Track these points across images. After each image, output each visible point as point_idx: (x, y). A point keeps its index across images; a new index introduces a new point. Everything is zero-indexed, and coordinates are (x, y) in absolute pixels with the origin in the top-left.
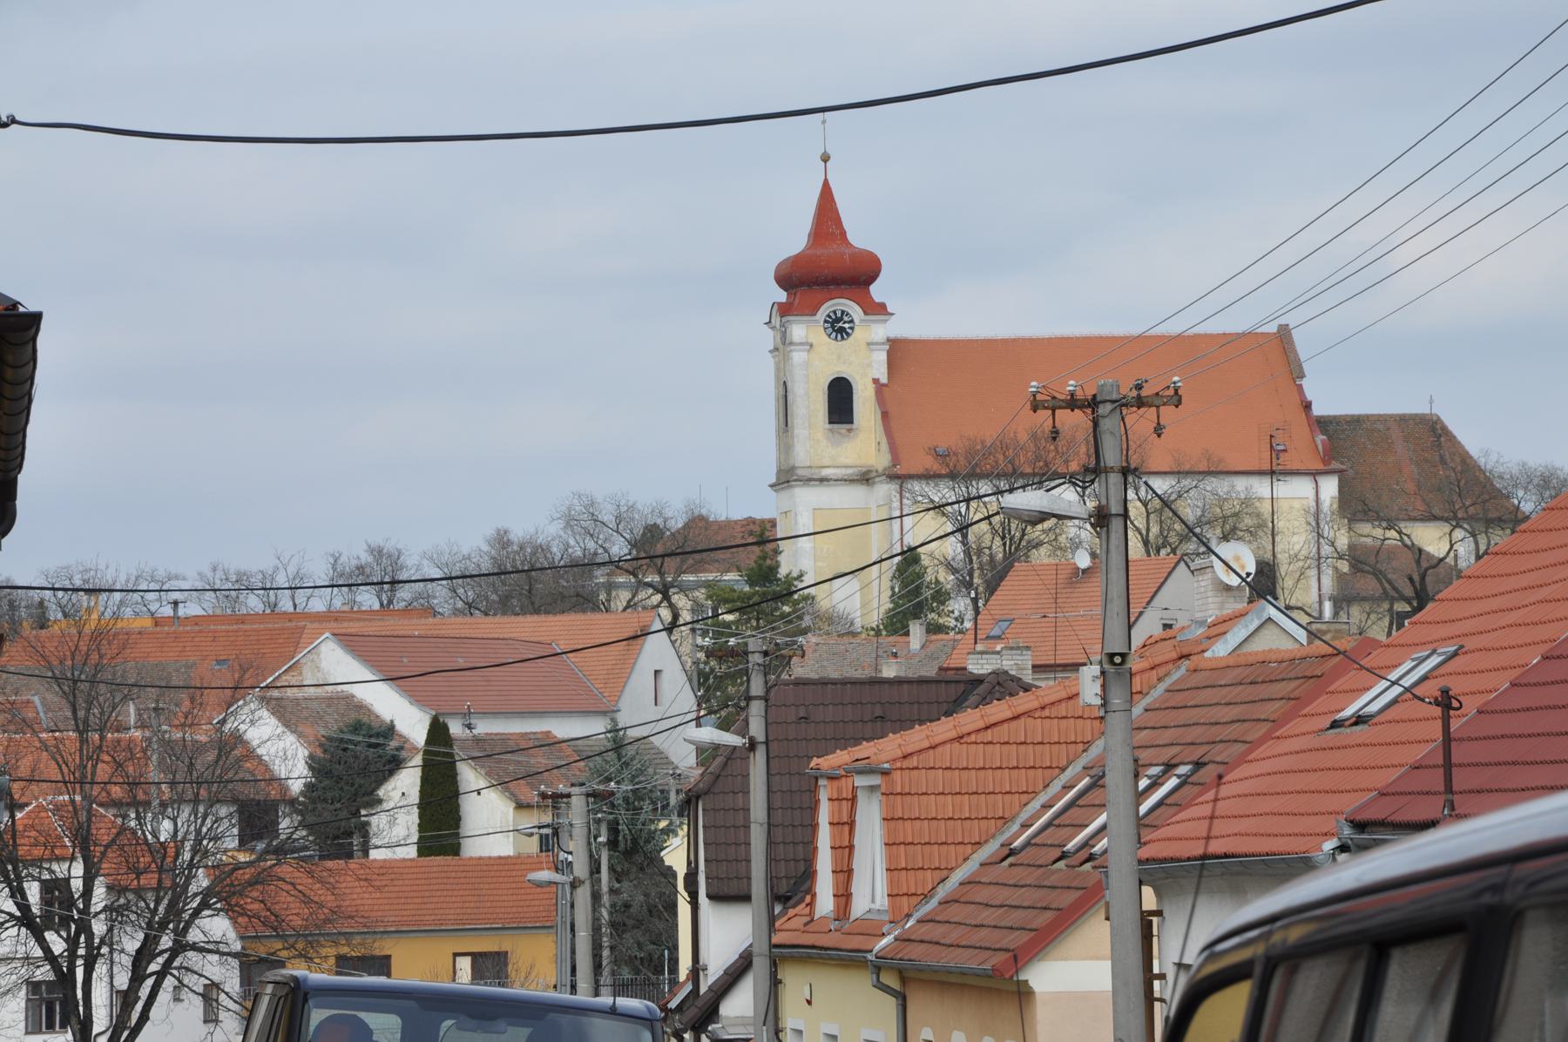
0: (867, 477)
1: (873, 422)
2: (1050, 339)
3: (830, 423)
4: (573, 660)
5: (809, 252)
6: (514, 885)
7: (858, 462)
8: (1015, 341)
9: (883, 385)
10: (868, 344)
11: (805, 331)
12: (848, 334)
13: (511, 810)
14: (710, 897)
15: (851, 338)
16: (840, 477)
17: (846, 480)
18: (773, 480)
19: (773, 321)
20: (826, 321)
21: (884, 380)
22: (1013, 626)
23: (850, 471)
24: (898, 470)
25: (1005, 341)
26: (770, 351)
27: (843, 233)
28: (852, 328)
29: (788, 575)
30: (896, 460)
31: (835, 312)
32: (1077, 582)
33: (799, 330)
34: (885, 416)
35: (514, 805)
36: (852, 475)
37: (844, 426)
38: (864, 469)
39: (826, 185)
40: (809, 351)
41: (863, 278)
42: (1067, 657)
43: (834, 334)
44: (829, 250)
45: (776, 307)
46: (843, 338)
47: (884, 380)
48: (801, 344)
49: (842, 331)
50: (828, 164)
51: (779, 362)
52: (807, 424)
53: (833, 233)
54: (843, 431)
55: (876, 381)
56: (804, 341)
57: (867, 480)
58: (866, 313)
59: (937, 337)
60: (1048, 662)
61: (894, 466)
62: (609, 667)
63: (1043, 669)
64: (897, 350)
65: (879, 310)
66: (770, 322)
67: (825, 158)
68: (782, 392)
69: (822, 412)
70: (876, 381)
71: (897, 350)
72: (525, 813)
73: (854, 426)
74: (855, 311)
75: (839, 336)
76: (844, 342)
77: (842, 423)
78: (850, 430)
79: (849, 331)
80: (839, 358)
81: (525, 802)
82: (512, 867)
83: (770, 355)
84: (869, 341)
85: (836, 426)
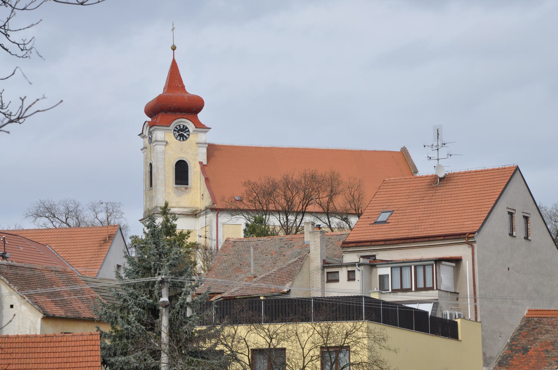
0: (195, 214)
1: (199, 185)
2: (288, 148)
3: (176, 184)
4: (62, 255)
5: (166, 94)
6: (60, 360)
7: (191, 206)
8: (270, 148)
9: (204, 165)
10: (197, 143)
11: (164, 135)
12: (186, 138)
13: (39, 320)
14: (372, 290)
15: (188, 140)
16: (181, 213)
17: (184, 215)
18: (142, 217)
19: (144, 132)
20: (175, 130)
21: (205, 163)
22: (393, 215)
23: (186, 210)
24: (215, 206)
25: (266, 149)
26: (142, 150)
27: (183, 87)
28: (189, 135)
29: (181, 233)
30: (214, 202)
31: (179, 126)
32: (437, 187)
33: (159, 134)
34: (207, 180)
35: (41, 315)
36: (187, 212)
37: (183, 186)
38: (194, 209)
39: (174, 62)
40: (165, 145)
41: (194, 109)
42: (443, 231)
43: (179, 137)
44: (177, 94)
45: (147, 123)
46: (183, 140)
47: (205, 163)
48: (161, 141)
49: (181, 136)
50: (175, 51)
51: (147, 154)
52: (164, 184)
53: (178, 86)
54: (183, 189)
55: (201, 163)
56: (163, 140)
57: (196, 215)
58: (196, 127)
59: (231, 145)
60: (319, 296)
61: (214, 204)
62: (88, 259)
63: (427, 239)
64: (212, 149)
65: (199, 125)
66: (142, 133)
67: (174, 48)
68: (148, 169)
69: (172, 178)
70: (201, 163)
71: (212, 149)
72: (50, 323)
73: (189, 186)
74: (191, 126)
75: (182, 138)
76: (184, 142)
77: (182, 184)
78: (186, 188)
79: (187, 136)
80: (181, 150)
81: (51, 314)
82: (57, 344)
83: (141, 152)
84: (198, 142)
85: (179, 186)
